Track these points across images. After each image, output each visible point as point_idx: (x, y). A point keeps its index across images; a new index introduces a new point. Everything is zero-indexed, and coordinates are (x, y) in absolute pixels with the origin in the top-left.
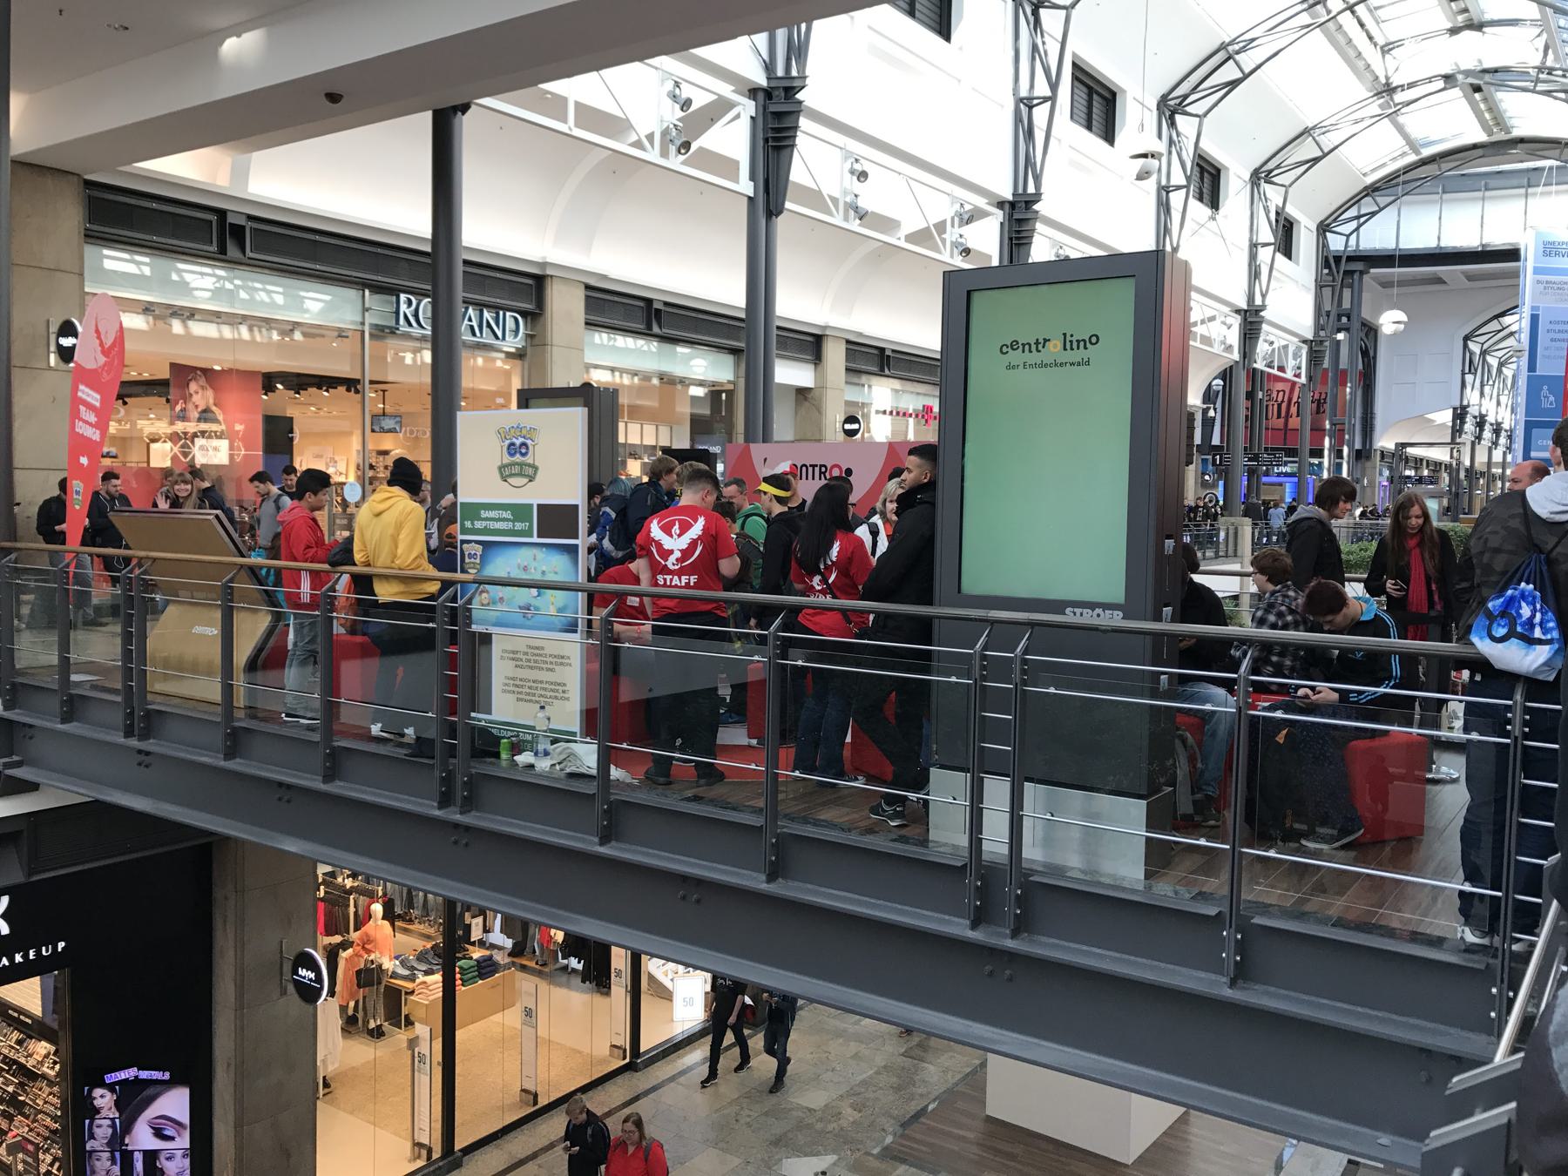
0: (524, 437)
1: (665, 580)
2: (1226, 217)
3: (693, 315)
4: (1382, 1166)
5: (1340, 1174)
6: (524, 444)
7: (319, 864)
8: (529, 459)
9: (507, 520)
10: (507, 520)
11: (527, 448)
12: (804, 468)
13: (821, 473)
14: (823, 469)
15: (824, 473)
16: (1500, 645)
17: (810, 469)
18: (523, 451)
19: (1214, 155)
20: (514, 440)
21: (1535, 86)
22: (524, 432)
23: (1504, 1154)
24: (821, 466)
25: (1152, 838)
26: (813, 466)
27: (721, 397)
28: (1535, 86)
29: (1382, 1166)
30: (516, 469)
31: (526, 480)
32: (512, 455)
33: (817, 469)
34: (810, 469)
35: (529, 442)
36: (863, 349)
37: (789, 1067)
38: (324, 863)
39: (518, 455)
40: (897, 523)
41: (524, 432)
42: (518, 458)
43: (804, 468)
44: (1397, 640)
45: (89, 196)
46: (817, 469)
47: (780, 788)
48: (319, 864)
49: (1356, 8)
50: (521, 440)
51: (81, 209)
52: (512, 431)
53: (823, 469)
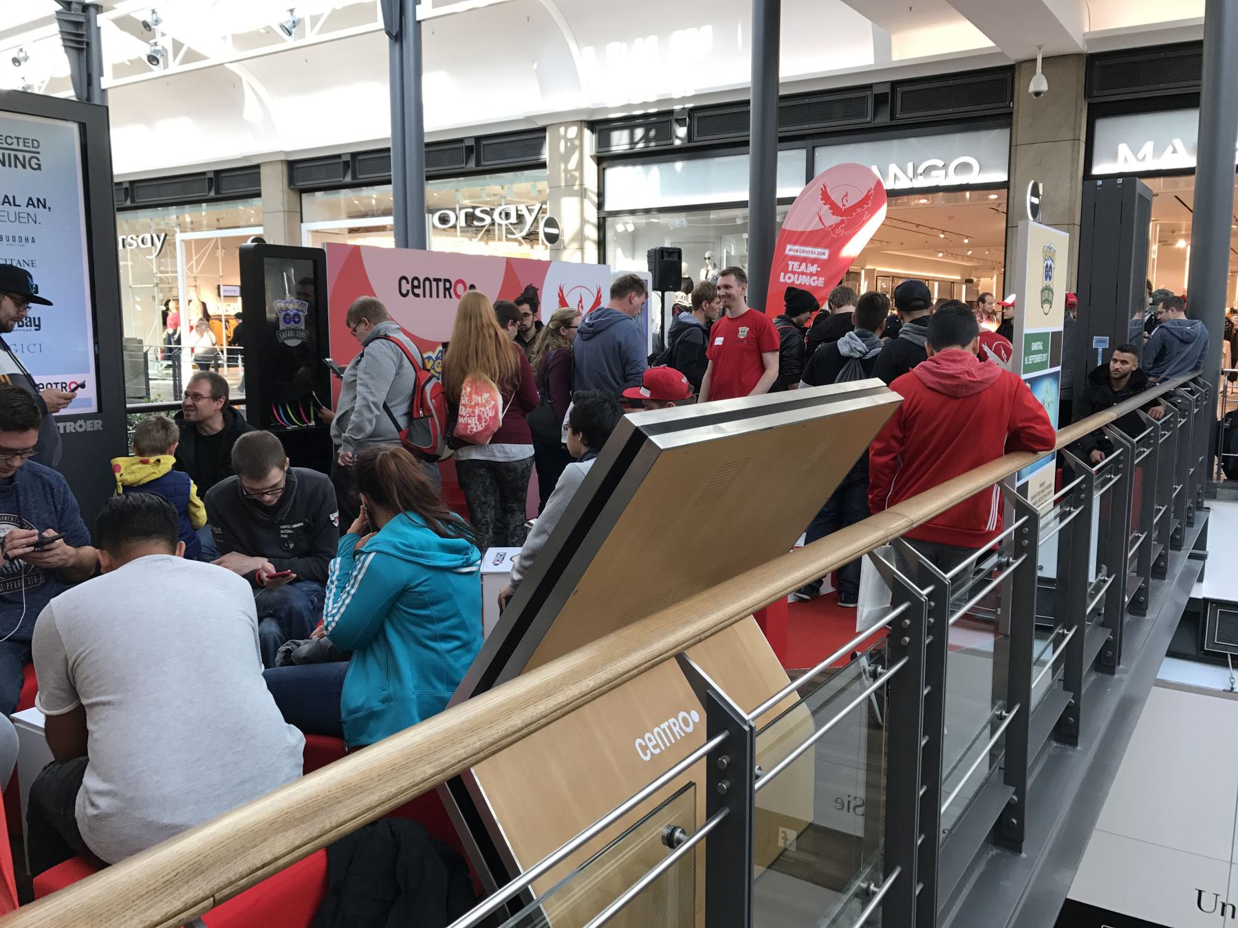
2: (686, 92)
5: (4, 262)
11: (300, 317)
12: (427, 283)
13: (445, 289)
15: (448, 290)
17: (434, 284)
18: (297, 320)
19: (704, 87)
23: (966, 757)
26: (438, 280)
33: (441, 284)
34: (434, 284)
36: (314, 164)
37: (270, 241)
39: (292, 323)
43: (427, 283)
44: (392, 173)
46: (441, 284)
47: (88, 422)
51: (152, 542)
53: (448, 285)
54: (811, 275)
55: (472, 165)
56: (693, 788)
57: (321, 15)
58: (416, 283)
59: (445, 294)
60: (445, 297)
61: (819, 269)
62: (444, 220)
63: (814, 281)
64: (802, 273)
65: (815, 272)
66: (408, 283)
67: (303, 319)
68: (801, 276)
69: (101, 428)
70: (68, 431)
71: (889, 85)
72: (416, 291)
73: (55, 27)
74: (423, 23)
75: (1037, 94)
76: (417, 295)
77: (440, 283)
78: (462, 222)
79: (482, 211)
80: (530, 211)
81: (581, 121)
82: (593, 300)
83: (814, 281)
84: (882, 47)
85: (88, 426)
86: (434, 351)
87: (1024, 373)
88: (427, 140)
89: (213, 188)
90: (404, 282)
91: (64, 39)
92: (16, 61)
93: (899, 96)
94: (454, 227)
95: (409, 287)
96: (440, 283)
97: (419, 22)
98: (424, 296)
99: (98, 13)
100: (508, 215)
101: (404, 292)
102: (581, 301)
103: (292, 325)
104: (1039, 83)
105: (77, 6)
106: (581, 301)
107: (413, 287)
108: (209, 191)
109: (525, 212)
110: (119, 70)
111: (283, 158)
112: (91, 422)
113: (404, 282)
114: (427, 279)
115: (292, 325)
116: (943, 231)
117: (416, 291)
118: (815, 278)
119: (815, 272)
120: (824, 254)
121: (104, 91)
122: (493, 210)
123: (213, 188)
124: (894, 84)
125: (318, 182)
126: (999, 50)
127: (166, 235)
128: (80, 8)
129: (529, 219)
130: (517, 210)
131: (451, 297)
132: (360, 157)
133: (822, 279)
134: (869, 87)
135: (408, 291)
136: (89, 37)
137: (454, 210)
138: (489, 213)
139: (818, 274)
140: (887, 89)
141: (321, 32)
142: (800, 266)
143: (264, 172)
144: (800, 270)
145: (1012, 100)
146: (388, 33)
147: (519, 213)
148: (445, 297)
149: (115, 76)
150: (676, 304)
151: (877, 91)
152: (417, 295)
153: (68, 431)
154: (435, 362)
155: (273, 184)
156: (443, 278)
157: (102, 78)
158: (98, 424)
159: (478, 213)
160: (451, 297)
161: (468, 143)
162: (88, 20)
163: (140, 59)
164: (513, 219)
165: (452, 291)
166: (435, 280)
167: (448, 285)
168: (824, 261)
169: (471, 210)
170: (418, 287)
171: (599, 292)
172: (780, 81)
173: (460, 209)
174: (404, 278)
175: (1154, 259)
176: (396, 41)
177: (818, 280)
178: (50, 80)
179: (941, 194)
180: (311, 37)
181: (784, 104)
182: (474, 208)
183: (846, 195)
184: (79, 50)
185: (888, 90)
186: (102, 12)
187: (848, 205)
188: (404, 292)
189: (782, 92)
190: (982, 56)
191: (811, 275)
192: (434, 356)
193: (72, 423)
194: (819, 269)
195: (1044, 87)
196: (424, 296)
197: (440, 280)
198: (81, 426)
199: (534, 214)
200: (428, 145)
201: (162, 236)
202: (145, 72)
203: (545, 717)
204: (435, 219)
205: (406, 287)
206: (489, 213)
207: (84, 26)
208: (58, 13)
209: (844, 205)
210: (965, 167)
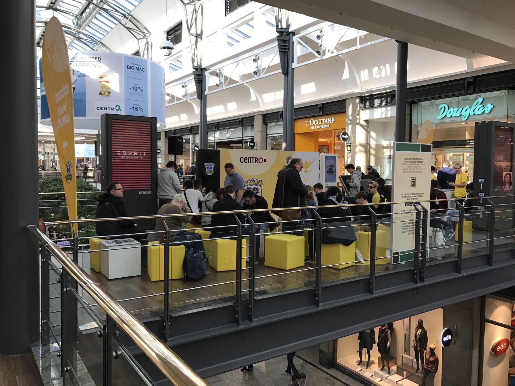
0: (256, 185)
3: (228, 122)
12: (250, 159)
13: (256, 160)
14: (256, 159)
15: (257, 160)
16: (118, 104)
17: (252, 159)
20: (250, 186)
22: (256, 182)
24: (256, 158)
25: (161, 379)
26: (253, 158)
27: (384, 196)
33: (254, 159)
34: (252, 159)
35: (259, 187)
36: (247, 119)
38: (412, 316)
40: (97, 138)
41: (256, 182)
43: (250, 159)
45: (198, 126)
46: (254, 159)
49: (138, 3)
50: (254, 186)
52: (249, 182)
53: (256, 159)
55: (321, 114)
57: (265, 68)
67: (213, 168)
71: (473, 78)
72: (246, 161)
73: (193, 77)
74: (295, 69)
81: (358, 97)
84: (470, 65)
88: (295, 108)
89: (321, 111)
90: (242, 158)
91: (195, 80)
92: (183, 87)
93: (478, 82)
95: (244, 160)
97: (293, 69)
98: (248, 162)
99: (205, 71)
101: (242, 161)
103: (210, 170)
105: (285, 34)
107: (245, 160)
108: (319, 113)
110: (211, 88)
113: (242, 158)
115: (210, 170)
116: (325, 146)
117: (246, 161)
121: (206, 95)
123: (321, 111)
125: (333, 112)
128: (200, 70)
131: (257, 163)
132: (220, 123)
134: (465, 79)
136: (289, 46)
140: (472, 80)
141: (265, 74)
143: (161, 133)
146: (283, 73)
148: (255, 162)
149: (209, 91)
151: (468, 80)
155: (258, 122)
160: (257, 163)
161: (319, 106)
162: (289, 39)
163: (251, 73)
166: (252, 158)
170: (247, 160)
172: (407, 83)
174: (242, 157)
175: (57, 160)
176: (286, 76)
178: (268, 67)
180: (262, 76)
181: (295, 111)
184: (199, 83)
185: (321, 106)
186: (207, 71)
188: (242, 161)
189: (208, 123)
190: (502, 66)
196: (248, 162)
200: (295, 109)
202: (253, 78)
205: (242, 160)
207: (201, 75)
208: (194, 72)
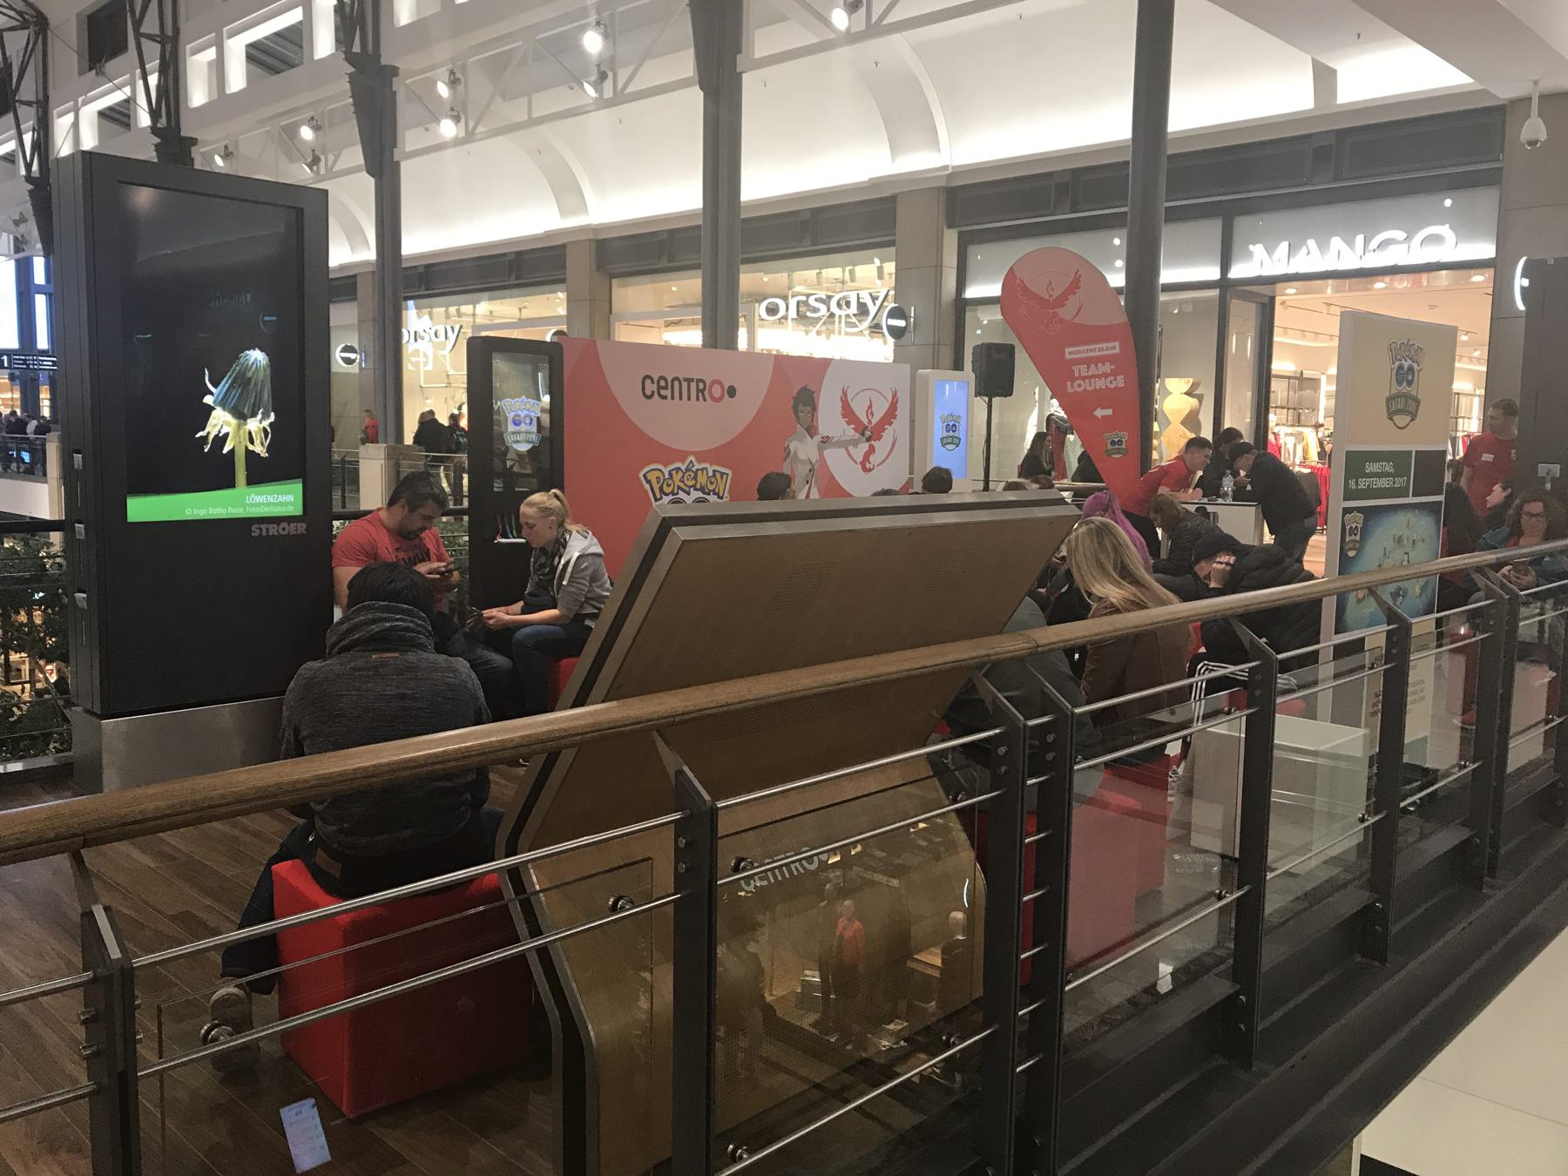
1: (261, 530)
4: (787, 876)
6: (954, 425)
7: (1493, 270)
8: (956, 434)
9: (1388, 475)
10: (1388, 475)
12: (676, 383)
13: (698, 390)
15: (702, 391)
17: (685, 385)
21: (150, 37)
26: (689, 381)
28: (150, 37)
29: (787, 876)
30: (950, 440)
31: (954, 446)
32: (948, 432)
33: (693, 385)
34: (685, 385)
42: (1117, 446)
43: (676, 383)
46: (693, 385)
48: (1493, 270)
53: (701, 386)
54: (1106, 375)
56: (650, 861)
58: (662, 383)
59: (698, 396)
60: (698, 399)
61: (1113, 367)
62: (772, 310)
63: (1111, 382)
64: (1094, 376)
65: (1109, 372)
66: (653, 382)
68: (1092, 380)
69: (304, 532)
70: (271, 534)
72: (663, 392)
75: (1532, 143)
76: (664, 398)
77: (692, 383)
78: (793, 313)
79: (816, 300)
80: (874, 299)
82: (887, 406)
83: (1111, 382)
85: (292, 529)
86: (683, 462)
87: (1441, 502)
90: (648, 382)
94: (785, 318)
95: (654, 387)
96: (692, 383)
98: (673, 398)
100: (848, 304)
101: (648, 393)
102: (870, 407)
104: (1534, 128)
106: (870, 407)
107: (659, 387)
109: (867, 300)
111: (591, 237)
112: (295, 525)
113: (648, 382)
114: (677, 379)
117: (663, 392)
118: (1112, 378)
119: (1109, 372)
120: (1114, 348)
122: (829, 297)
124: (1342, 133)
126: (1479, 87)
127: (461, 327)
129: (873, 310)
130: (858, 298)
131: (705, 400)
133: (1120, 378)
135: (653, 392)
137: (785, 298)
138: (826, 301)
139: (1114, 374)
142: (1088, 368)
144: (1090, 374)
145: (1502, 151)
147: (861, 301)
148: (698, 399)
150: (1051, 415)
152: (664, 398)
153: (271, 534)
154: (684, 474)
156: (695, 377)
157: (395, 149)
158: (302, 527)
159: (812, 301)
160: (705, 400)
164: (854, 309)
165: (706, 393)
166: (685, 380)
167: (701, 386)
168: (1115, 356)
169: (804, 298)
171: (895, 395)
173: (793, 296)
177: (1115, 379)
179: (1444, 272)
182: (808, 296)
183: (1050, 284)
187: (1056, 294)
188: (648, 393)
191: (1106, 375)
192: (683, 468)
193: (275, 526)
194: (1113, 367)
195: (1542, 135)
196: (673, 398)
197: (692, 380)
198: (284, 529)
199: (878, 303)
201: (457, 328)
203: (439, 763)
204: (761, 309)
205: (651, 387)
206: (826, 301)
209: (1051, 296)
210: (1436, 239)
